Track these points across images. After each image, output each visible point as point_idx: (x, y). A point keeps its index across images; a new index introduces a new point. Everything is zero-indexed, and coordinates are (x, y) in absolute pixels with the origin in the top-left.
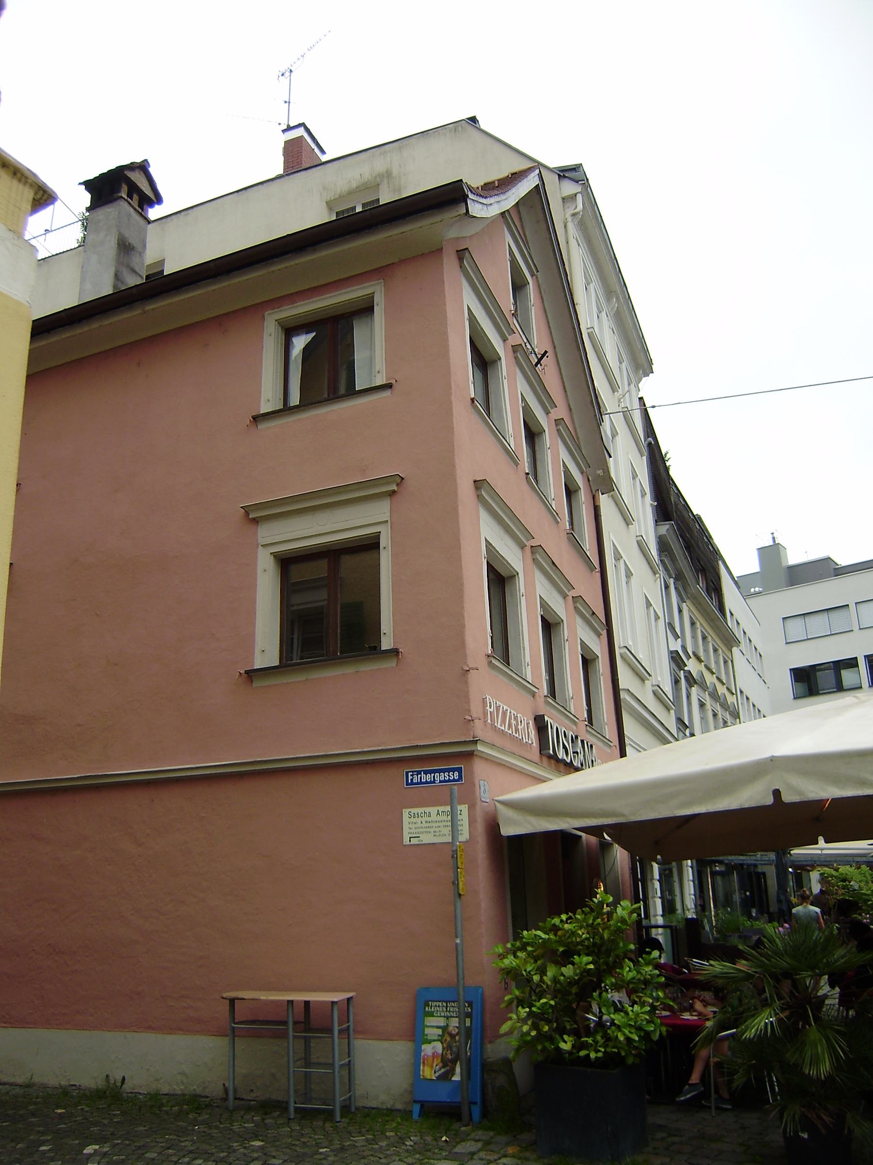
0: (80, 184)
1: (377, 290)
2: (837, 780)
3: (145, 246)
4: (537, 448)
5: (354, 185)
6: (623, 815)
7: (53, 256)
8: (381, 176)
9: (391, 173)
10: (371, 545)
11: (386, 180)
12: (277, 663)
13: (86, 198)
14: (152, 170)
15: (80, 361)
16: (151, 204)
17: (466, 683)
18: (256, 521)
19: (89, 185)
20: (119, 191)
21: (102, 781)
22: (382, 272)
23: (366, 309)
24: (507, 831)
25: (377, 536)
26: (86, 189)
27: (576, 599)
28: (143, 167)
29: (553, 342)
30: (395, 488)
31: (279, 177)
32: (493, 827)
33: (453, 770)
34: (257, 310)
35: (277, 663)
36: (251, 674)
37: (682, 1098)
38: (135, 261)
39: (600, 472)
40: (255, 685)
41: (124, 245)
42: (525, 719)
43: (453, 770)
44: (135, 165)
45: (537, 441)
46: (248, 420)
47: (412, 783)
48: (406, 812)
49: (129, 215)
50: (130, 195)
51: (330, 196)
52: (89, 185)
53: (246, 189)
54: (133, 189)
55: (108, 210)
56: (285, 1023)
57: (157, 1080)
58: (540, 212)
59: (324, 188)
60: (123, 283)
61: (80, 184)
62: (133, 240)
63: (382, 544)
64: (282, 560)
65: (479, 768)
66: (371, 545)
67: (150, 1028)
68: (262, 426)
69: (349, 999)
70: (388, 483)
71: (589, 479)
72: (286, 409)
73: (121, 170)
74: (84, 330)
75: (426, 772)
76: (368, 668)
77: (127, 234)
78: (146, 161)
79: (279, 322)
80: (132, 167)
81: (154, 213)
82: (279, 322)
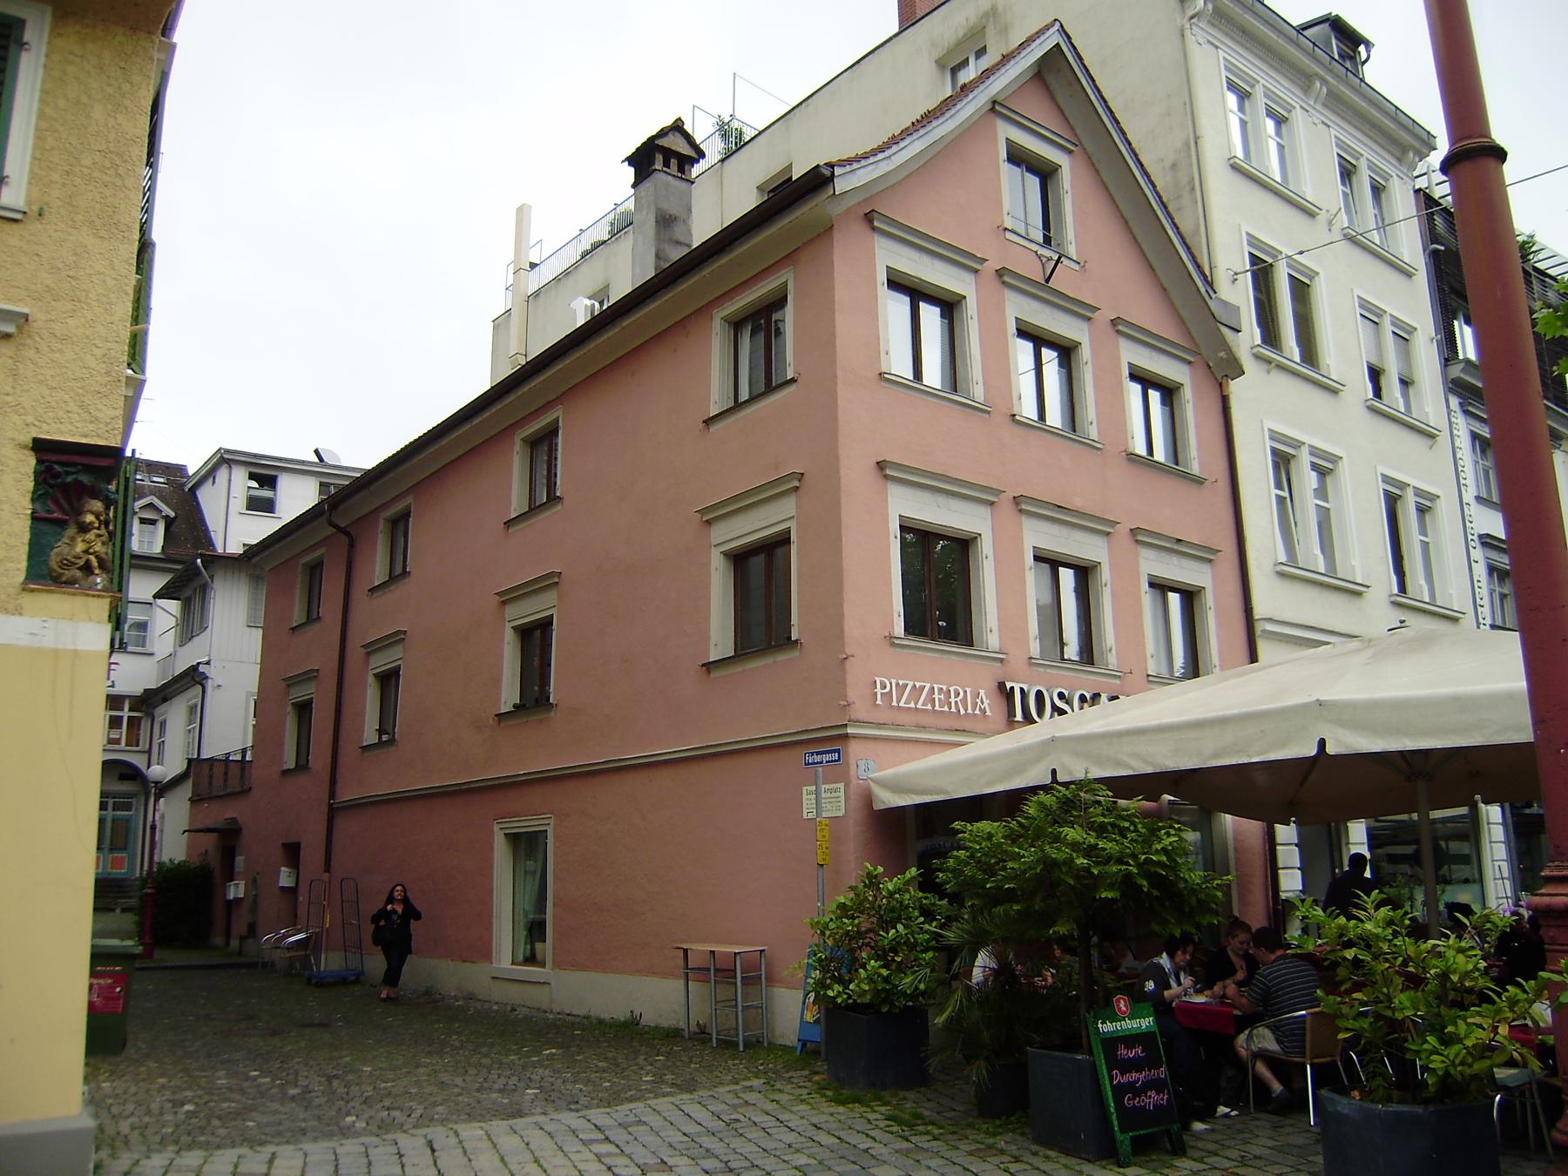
0: (623, 162)
1: (786, 276)
2: (1373, 730)
3: (690, 210)
4: (1073, 365)
5: (961, 34)
6: (946, 792)
7: (760, 133)
8: (986, 15)
9: (997, 9)
10: (783, 540)
11: (991, 19)
12: (732, 654)
13: (629, 173)
14: (688, 127)
15: (594, 376)
16: (693, 161)
17: (844, 670)
18: (709, 523)
19: (631, 160)
20: (654, 164)
21: (603, 767)
22: (789, 259)
23: (779, 302)
24: (878, 806)
25: (788, 531)
26: (629, 164)
27: (1135, 532)
28: (677, 127)
29: (1122, 216)
30: (796, 484)
31: (896, 35)
32: (868, 799)
33: (834, 751)
34: (705, 310)
35: (732, 654)
36: (709, 666)
37: (1080, 1057)
38: (678, 233)
39: (1222, 354)
40: (712, 676)
41: (664, 218)
42: (968, 690)
43: (834, 751)
44: (666, 130)
45: (1072, 356)
46: (702, 425)
47: (809, 764)
48: (805, 788)
49: (668, 185)
50: (666, 164)
51: (937, 54)
52: (631, 160)
53: (858, 62)
54: (668, 154)
55: (647, 185)
56: (709, 969)
57: (660, 1016)
58: (1069, 74)
59: (933, 44)
60: (666, 260)
61: (623, 162)
62: (673, 208)
63: (793, 537)
64: (735, 556)
65: (855, 750)
66: (783, 540)
67: (655, 974)
68: (714, 428)
69: (761, 951)
70: (790, 481)
71: (1208, 365)
72: (738, 406)
73: (651, 140)
74: (474, 423)
75: (818, 753)
76: (782, 657)
77: (665, 206)
78: (679, 119)
79: (725, 319)
80: (663, 133)
81: (696, 170)
82: (725, 319)
